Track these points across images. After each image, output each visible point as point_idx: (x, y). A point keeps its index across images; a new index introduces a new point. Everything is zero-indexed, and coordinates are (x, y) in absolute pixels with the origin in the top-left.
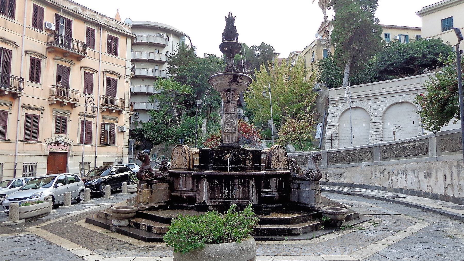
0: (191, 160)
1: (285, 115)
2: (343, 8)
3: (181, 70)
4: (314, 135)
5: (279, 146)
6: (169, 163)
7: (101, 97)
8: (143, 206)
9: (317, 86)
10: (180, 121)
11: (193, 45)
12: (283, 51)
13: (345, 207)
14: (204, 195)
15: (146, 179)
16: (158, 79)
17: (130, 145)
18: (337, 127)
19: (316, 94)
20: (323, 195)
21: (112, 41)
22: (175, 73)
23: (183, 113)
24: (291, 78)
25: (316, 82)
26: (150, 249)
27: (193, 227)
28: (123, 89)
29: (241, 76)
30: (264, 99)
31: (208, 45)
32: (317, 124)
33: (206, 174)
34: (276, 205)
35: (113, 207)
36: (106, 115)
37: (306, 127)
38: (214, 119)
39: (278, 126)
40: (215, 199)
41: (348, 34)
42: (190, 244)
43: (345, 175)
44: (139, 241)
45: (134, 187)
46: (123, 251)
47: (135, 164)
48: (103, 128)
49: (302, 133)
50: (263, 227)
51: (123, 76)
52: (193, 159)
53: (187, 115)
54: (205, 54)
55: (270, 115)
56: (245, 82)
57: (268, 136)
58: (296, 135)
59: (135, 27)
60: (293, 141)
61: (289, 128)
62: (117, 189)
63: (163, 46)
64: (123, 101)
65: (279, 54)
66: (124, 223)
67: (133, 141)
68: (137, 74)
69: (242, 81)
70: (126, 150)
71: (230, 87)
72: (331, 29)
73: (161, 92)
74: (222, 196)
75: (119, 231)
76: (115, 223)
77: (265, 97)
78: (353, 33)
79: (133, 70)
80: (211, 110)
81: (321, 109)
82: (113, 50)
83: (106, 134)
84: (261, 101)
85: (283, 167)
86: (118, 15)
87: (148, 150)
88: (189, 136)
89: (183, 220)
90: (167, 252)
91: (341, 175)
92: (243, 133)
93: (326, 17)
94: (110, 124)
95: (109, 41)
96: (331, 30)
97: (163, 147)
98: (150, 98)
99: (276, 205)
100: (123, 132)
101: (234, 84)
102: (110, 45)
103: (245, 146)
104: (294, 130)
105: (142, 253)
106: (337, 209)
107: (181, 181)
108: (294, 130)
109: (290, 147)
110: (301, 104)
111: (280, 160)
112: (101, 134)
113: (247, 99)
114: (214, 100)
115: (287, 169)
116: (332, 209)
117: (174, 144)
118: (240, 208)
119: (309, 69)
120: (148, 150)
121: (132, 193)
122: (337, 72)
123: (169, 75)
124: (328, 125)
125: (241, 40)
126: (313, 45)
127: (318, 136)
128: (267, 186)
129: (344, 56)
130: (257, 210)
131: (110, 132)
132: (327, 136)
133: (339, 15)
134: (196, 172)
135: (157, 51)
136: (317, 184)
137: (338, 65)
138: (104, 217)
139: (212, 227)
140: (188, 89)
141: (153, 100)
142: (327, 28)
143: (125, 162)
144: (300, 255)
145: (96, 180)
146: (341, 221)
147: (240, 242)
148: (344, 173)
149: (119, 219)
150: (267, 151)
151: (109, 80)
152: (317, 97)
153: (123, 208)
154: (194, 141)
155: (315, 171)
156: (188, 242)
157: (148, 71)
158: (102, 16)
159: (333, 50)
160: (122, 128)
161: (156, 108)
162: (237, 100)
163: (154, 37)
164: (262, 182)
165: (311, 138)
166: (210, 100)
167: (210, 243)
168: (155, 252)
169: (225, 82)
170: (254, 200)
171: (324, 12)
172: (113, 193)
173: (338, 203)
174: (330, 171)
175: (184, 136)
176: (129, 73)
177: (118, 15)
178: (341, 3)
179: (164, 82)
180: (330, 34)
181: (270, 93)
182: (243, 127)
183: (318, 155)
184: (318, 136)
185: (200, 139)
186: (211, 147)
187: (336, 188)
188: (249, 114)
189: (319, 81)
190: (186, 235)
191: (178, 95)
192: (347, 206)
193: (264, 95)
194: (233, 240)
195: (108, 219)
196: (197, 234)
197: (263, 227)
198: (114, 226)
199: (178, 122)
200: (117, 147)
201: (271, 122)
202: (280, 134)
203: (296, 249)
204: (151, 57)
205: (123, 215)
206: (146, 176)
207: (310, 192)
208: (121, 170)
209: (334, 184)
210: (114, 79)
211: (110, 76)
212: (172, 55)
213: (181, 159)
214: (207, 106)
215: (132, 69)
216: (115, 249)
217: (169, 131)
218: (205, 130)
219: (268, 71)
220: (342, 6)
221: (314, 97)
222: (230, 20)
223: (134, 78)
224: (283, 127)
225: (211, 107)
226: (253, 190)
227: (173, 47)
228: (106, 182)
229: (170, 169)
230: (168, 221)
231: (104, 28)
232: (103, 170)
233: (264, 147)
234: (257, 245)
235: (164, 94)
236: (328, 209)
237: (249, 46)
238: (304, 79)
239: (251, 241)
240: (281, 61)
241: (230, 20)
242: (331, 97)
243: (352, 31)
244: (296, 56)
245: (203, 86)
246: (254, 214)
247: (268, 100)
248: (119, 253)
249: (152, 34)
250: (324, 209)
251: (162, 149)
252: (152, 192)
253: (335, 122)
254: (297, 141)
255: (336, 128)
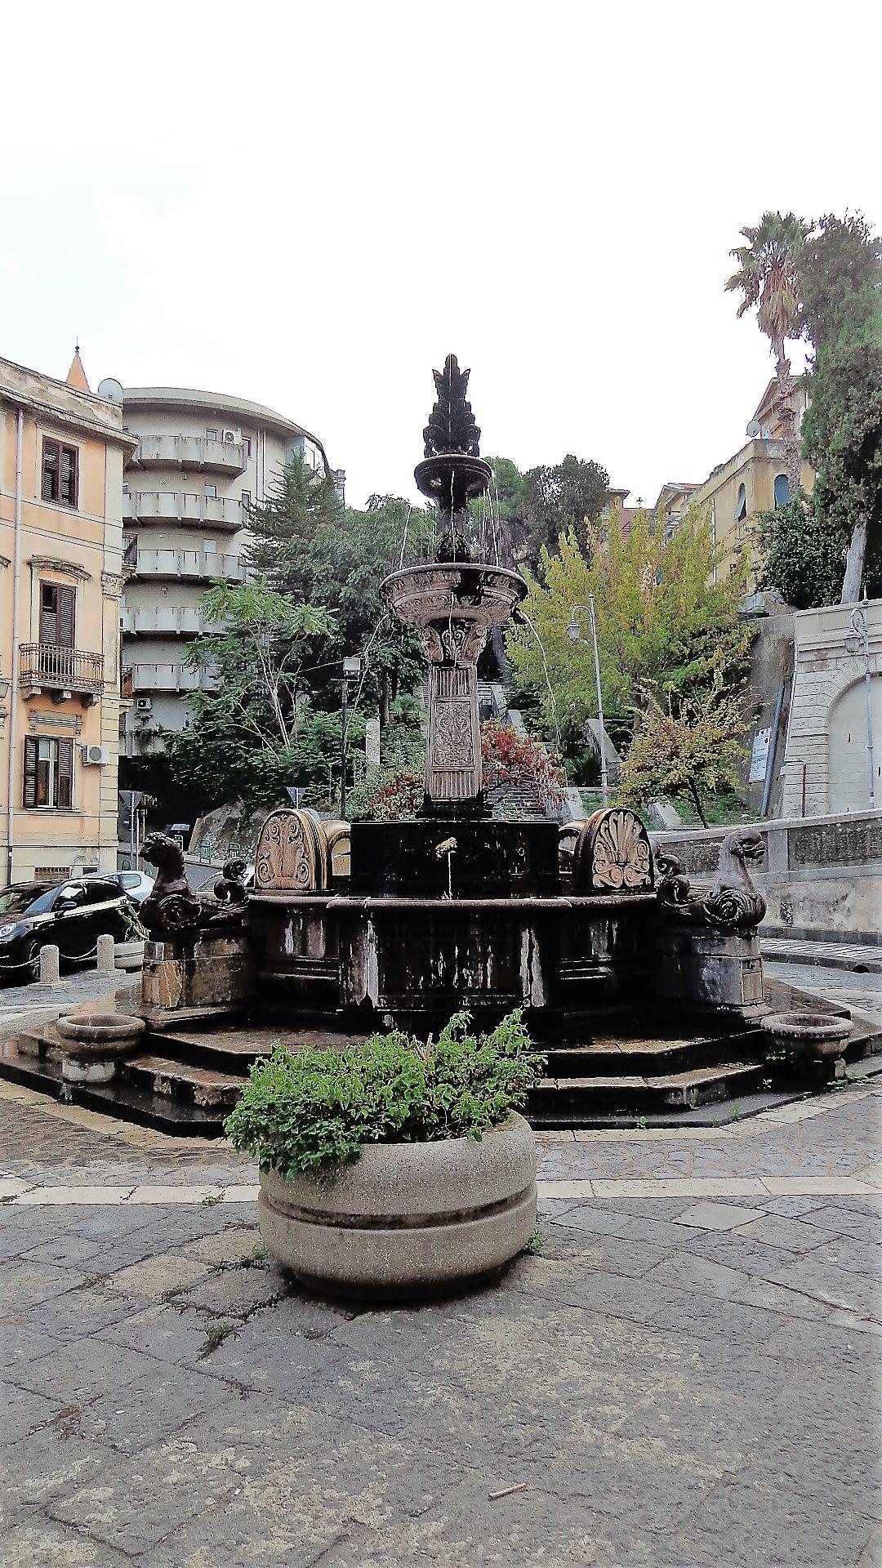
0: (322, 863)
1: (644, 705)
2: (844, 333)
3: (290, 556)
4: (745, 771)
5: (618, 812)
6: (250, 871)
7: (25, 650)
8: (163, 1017)
9: (756, 603)
10: (289, 728)
11: (333, 467)
12: (639, 481)
13: (846, 1015)
14: (368, 979)
15: (174, 924)
16: (213, 585)
17: (124, 814)
18: (822, 740)
19: (749, 629)
20: (771, 971)
21: (57, 461)
22: (270, 564)
23: (301, 701)
24: (667, 573)
25: (752, 587)
26: (186, 1157)
27: (322, 1090)
28: (98, 622)
29: (487, 574)
30: (575, 649)
31: (379, 465)
32: (754, 732)
33: (371, 908)
34: (611, 1010)
35: (64, 1021)
36: (44, 708)
37: (715, 742)
38: (403, 719)
39: (620, 739)
40: (404, 992)
41: (860, 421)
42: (314, 1147)
43: (847, 903)
44: (151, 1132)
45: (135, 949)
46: (94, 1166)
47: (141, 873)
48: (32, 756)
49: (699, 767)
50: (564, 1083)
51: (96, 575)
52: (329, 856)
53: (315, 705)
54: (373, 498)
55: (594, 705)
56: (503, 595)
57: (587, 775)
58: (680, 771)
59: (138, 408)
60: (672, 790)
61: (659, 746)
62: (84, 957)
63: (231, 474)
64: (98, 661)
65: (624, 494)
66: (100, 1072)
67: (136, 797)
68: (144, 567)
69: (494, 592)
70: (111, 826)
71: (450, 613)
72: (802, 405)
73: (227, 629)
74: (428, 979)
75: (83, 1096)
76: (72, 1071)
77: (576, 642)
78: (876, 420)
79: (130, 553)
80: (394, 689)
81: (767, 677)
82: (63, 489)
83: (41, 774)
84: (564, 658)
85: (635, 880)
86: (77, 368)
87: (185, 827)
88: (328, 773)
89: (293, 1066)
90: (243, 1167)
91: (835, 904)
92: (500, 765)
93: (783, 366)
94: (56, 740)
95: (50, 458)
96: (803, 410)
97: (236, 815)
98: (188, 650)
99: (611, 1010)
100: (99, 766)
101: (466, 601)
102: (50, 471)
103: (504, 813)
104: (675, 754)
105: (159, 1170)
106: (816, 1023)
107: (288, 932)
108: (675, 754)
109: (665, 811)
110: (698, 666)
111: (623, 858)
112: (27, 774)
113: (513, 652)
114: (407, 655)
115: (648, 888)
116: (800, 1021)
117: (269, 805)
118: (484, 1023)
119: (728, 545)
120: (185, 827)
121: (130, 970)
122: (825, 555)
123: (253, 571)
124: (790, 732)
125: (489, 447)
126: (740, 463)
127: (759, 772)
128: (582, 946)
129: (847, 496)
130: (540, 1026)
131: (56, 764)
132: (790, 775)
133: (830, 356)
134: (338, 900)
135: (210, 491)
136: (748, 938)
137: (829, 531)
138: (36, 1051)
139: (388, 1090)
140: (317, 620)
141: (198, 657)
142: (787, 403)
143: (108, 868)
144: (687, 1176)
145: (11, 927)
146: (832, 1057)
147: (478, 1138)
148: (844, 898)
149: (84, 1058)
150: (581, 826)
151: (49, 595)
152: (755, 640)
153: (97, 1022)
154: (338, 795)
155: (740, 893)
156: (305, 1137)
157: (181, 559)
158: (23, 372)
159: (808, 479)
160: (97, 752)
161: (210, 685)
162: (477, 655)
163: (198, 440)
164: (562, 935)
165: (734, 783)
166: (387, 654)
167: (382, 1140)
168: (203, 1167)
169: (437, 597)
170: (535, 993)
171: (778, 349)
172: (67, 969)
173: (820, 1002)
174: (797, 891)
175: (303, 780)
176: (115, 564)
177: (77, 368)
178: (836, 316)
179: (236, 597)
180: (799, 421)
181: (593, 628)
182: (503, 750)
183: (751, 841)
184: (759, 772)
185: (359, 788)
186: (392, 816)
187: (820, 950)
188: (523, 701)
189: (762, 586)
190: (299, 1116)
191: (283, 643)
192: (852, 1010)
193: (574, 634)
194: (457, 1128)
195: (50, 1060)
196: (336, 1111)
197: (564, 1083)
198: (66, 1081)
199: (283, 727)
200: (80, 816)
201: (597, 727)
202: (627, 768)
203: (674, 1156)
204: (192, 512)
205: (94, 1046)
206: (173, 917)
207: (726, 964)
208: (96, 893)
209: (812, 936)
210: (68, 588)
211: (53, 578)
212: (260, 504)
213: (288, 857)
214: (382, 676)
215: (127, 552)
216: (70, 1159)
217: (255, 761)
218: (373, 756)
219: (585, 552)
220: (839, 324)
221: (745, 642)
222: (451, 382)
223: (136, 582)
224: (637, 741)
225: (394, 679)
226: (530, 960)
227: (263, 475)
228: (44, 935)
229: (254, 893)
230: (238, 1065)
231: (31, 414)
232: (36, 893)
233: (575, 810)
234: (548, 1145)
235: (235, 636)
236: (788, 1021)
237: (524, 467)
238: (711, 580)
239: (519, 1129)
240: (633, 520)
241: (451, 382)
242: (800, 640)
243: (872, 412)
244: (682, 500)
245: (366, 607)
246: (528, 1042)
247: (588, 651)
248: (82, 1171)
249: (193, 431)
250: (774, 1023)
251: (231, 822)
252: (191, 970)
253: (816, 725)
254: (683, 792)
255: (819, 746)
